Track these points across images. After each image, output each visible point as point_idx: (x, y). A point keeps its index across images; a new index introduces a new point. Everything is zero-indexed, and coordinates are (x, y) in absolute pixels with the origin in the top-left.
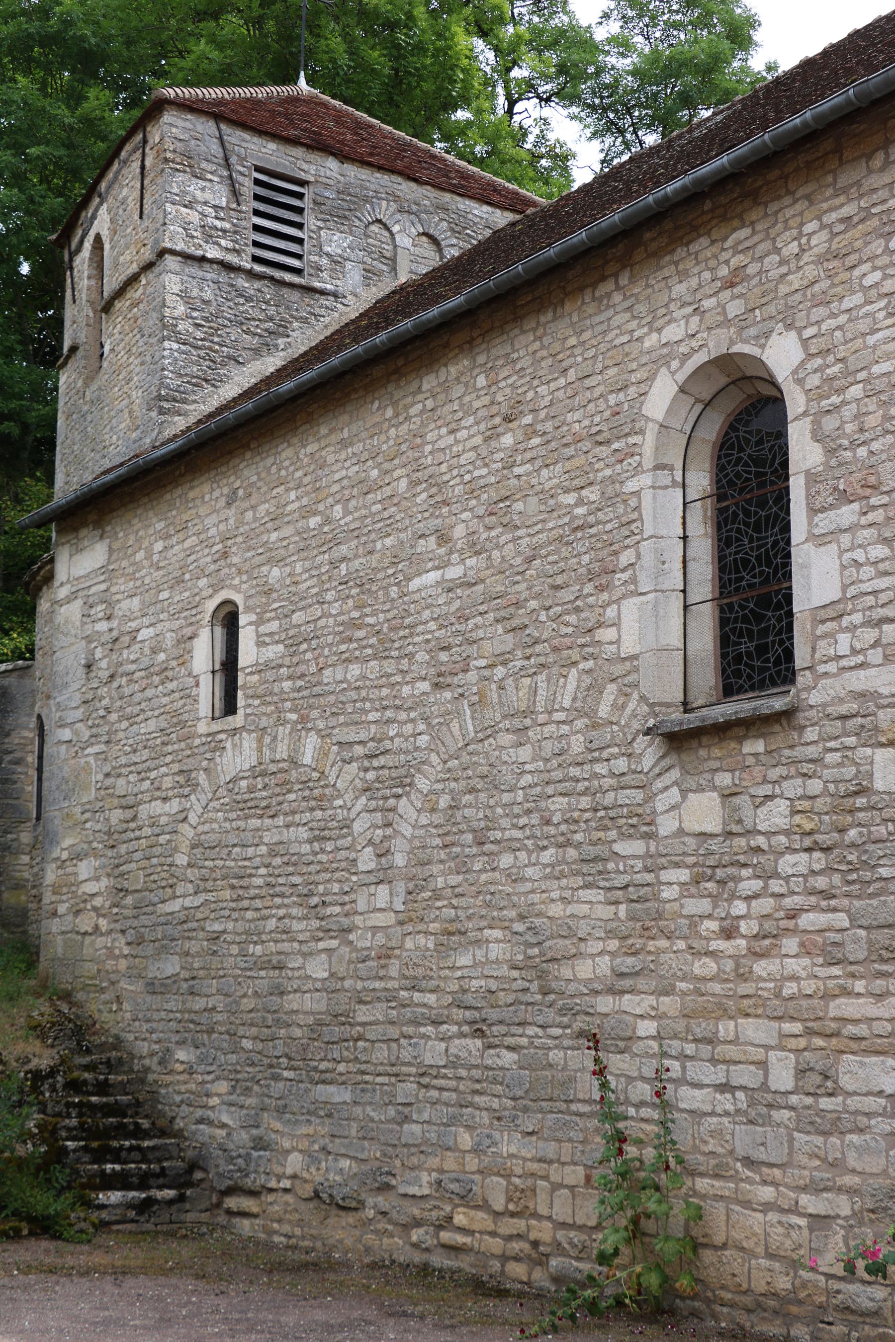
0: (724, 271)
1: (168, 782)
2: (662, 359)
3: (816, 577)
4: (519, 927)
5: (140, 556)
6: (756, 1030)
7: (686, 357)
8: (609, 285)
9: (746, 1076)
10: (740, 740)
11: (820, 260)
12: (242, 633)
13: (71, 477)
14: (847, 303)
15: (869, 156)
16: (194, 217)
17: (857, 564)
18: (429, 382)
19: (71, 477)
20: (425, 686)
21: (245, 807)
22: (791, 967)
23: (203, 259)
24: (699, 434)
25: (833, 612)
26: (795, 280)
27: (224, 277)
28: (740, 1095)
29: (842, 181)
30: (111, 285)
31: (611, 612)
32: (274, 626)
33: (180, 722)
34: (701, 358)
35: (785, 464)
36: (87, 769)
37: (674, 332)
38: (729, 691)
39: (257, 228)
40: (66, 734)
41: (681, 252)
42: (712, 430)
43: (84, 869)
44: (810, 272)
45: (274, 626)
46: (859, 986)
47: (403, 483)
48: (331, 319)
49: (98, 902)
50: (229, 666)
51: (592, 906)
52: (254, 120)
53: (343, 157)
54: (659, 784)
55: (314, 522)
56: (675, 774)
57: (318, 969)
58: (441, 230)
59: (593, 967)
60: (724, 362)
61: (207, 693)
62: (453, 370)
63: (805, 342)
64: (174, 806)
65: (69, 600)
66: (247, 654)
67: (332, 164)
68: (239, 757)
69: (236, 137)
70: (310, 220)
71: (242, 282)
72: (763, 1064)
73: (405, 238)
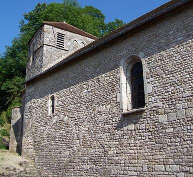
0: (132, 43)
1: (43, 124)
2: (122, 57)
3: (148, 88)
4: (101, 146)
5: (39, 89)
6: (141, 161)
7: (126, 56)
8: (114, 46)
9: (139, 169)
10: (137, 115)
11: (146, 42)
12: (55, 101)
13: (31, 74)
14: (151, 48)
15: (153, 27)
16: (48, 39)
17: (154, 87)
18: (85, 61)
19: (31, 74)
20: (85, 108)
21: (55, 128)
22: (146, 151)
23: (49, 45)
24: (128, 68)
25: (150, 94)
26: (143, 45)
27: (53, 48)
28: (138, 172)
29: (149, 30)
30: (36, 49)
31: (115, 95)
32: (60, 99)
33: (46, 114)
34: (128, 56)
35: (142, 72)
36: (30, 122)
37: (124, 53)
38: (133, 108)
39: (58, 41)
40: (27, 117)
41: (125, 41)
42: (130, 67)
43: (29, 138)
44: (145, 43)
45: (60, 99)
46: (158, 153)
47: (81, 77)
48: (68, 54)
49: (31, 143)
50: (53, 106)
51: (113, 143)
52: (57, 26)
53: (70, 32)
54: (124, 122)
55: (67, 83)
56: (126, 121)
57: (67, 153)
58: (85, 42)
59: (112, 152)
60: (132, 57)
61: (50, 110)
62: (89, 59)
63: (145, 53)
64: (44, 128)
65: (28, 96)
66: (56, 103)
67: (69, 32)
68: (55, 120)
69: (54, 28)
70: (65, 40)
71: (55, 49)
72: (142, 167)
73: (79, 42)
